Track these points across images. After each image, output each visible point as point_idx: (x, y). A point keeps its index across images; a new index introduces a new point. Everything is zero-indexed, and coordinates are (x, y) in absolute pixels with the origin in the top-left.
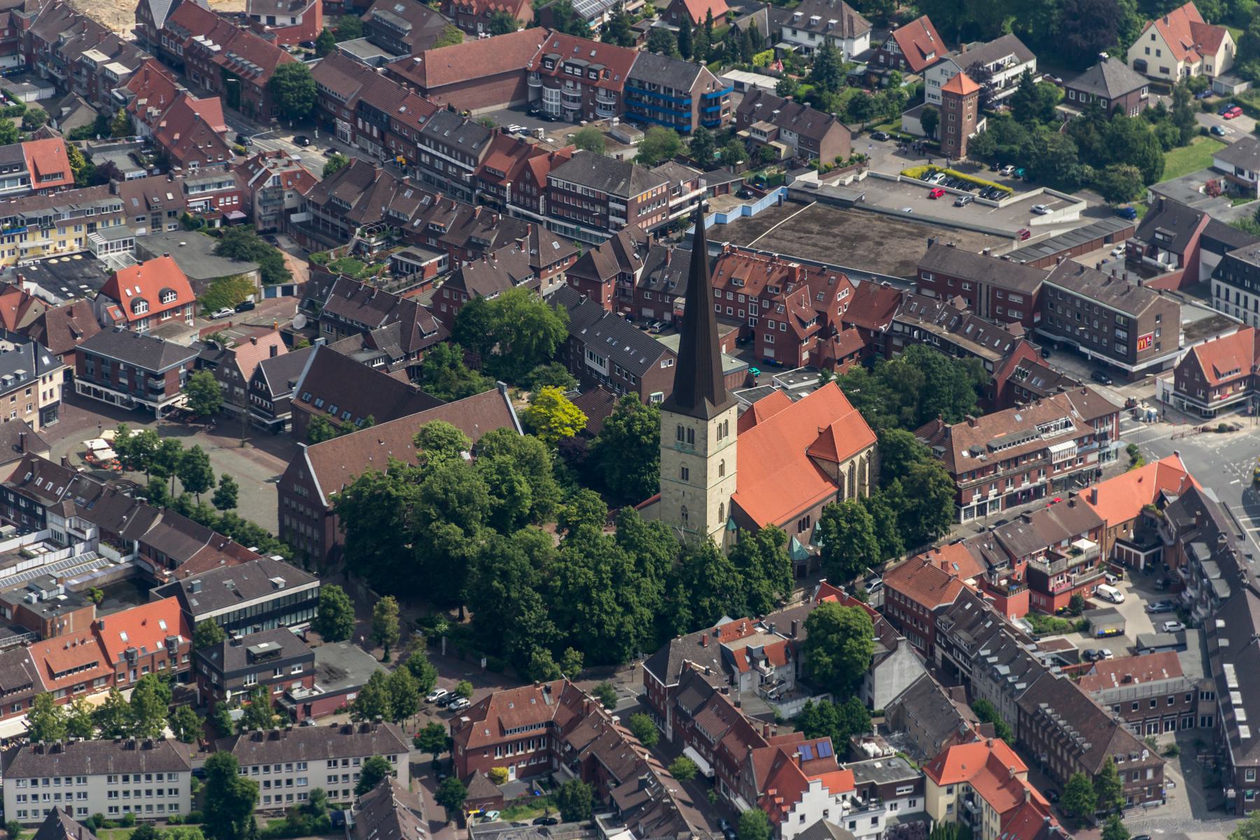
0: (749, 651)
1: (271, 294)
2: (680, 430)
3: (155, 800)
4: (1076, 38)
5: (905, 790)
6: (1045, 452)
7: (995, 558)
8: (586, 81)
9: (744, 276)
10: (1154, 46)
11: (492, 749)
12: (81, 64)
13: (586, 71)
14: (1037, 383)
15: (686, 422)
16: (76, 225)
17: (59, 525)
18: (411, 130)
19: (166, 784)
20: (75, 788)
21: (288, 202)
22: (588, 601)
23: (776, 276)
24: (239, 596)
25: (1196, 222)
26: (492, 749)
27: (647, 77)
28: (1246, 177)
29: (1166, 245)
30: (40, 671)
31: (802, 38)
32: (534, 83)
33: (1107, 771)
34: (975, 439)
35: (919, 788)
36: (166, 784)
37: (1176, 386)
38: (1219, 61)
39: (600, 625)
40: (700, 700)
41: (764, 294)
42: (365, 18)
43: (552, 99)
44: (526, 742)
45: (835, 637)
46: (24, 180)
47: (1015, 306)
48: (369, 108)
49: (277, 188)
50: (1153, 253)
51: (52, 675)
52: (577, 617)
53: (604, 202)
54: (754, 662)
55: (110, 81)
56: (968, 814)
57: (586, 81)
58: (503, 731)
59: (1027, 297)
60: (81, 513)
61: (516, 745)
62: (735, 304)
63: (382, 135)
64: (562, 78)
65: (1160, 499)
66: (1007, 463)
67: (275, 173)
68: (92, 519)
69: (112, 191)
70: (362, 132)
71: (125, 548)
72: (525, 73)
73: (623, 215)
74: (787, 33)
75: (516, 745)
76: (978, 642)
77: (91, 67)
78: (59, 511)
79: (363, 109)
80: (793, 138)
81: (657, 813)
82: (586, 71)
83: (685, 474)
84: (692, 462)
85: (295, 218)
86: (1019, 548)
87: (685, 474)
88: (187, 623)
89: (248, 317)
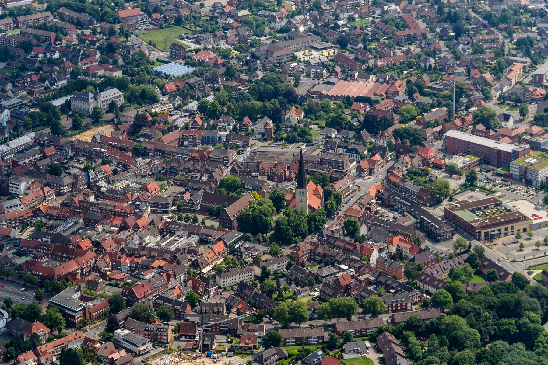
0: (336, 230)
1: (169, 186)
2: (300, 193)
3: (248, 277)
4: (276, 115)
5: (386, 248)
6: (349, 187)
7: (361, 206)
8: (193, 138)
9: (265, 166)
10: (291, 115)
11: (302, 256)
12: (93, 151)
13: (193, 136)
14: (338, 176)
15: (301, 190)
16: (124, 180)
17: (177, 233)
18: (170, 152)
19: (250, 274)
20: (233, 278)
21: (159, 169)
22: (299, 227)
23: (272, 165)
24: (232, 238)
25: (336, 143)
26: (302, 256)
27: (207, 135)
28: (329, 135)
29: (331, 148)
30: (206, 258)
31: (223, 124)
32: (182, 140)
33: (418, 238)
34: (339, 186)
35: (388, 247)
36: (250, 274)
37: (356, 172)
38: (302, 116)
39: (302, 231)
40: (334, 240)
41: (271, 169)
42: (140, 133)
43: (186, 143)
44: (307, 254)
45: (353, 224)
46: (104, 174)
47: (316, 164)
48: (158, 150)
49: (157, 167)
50: (328, 150)
51: (209, 259)
52: (298, 230)
53: (223, 159)
54: (338, 232)
55: (103, 153)
56: (399, 250)
57: (193, 138)
58: (304, 252)
59: (318, 161)
60: (183, 230)
61: (305, 255)
62: (265, 172)
63: (163, 154)
64: (188, 138)
65: (378, 191)
66: (344, 190)
67: (156, 163)
68: (187, 230)
69: (128, 172)
70: (157, 155)
71: (198, 234)
72: (179, 139)
73: (228, 160)
74: (219, 124)
75: (305, 255)
76: (373, 221)
77: (96, 151)
78: (178, 230)
79: (156, 150)
80: (242, 142)
81: (348, 260)
82: (193, 136)
83: (301, 200)
84: (303, 198)
85: (162, 172)
86: (364, 204)
87: (301, 200)
88: (226, 244)
89: (167, 191)
